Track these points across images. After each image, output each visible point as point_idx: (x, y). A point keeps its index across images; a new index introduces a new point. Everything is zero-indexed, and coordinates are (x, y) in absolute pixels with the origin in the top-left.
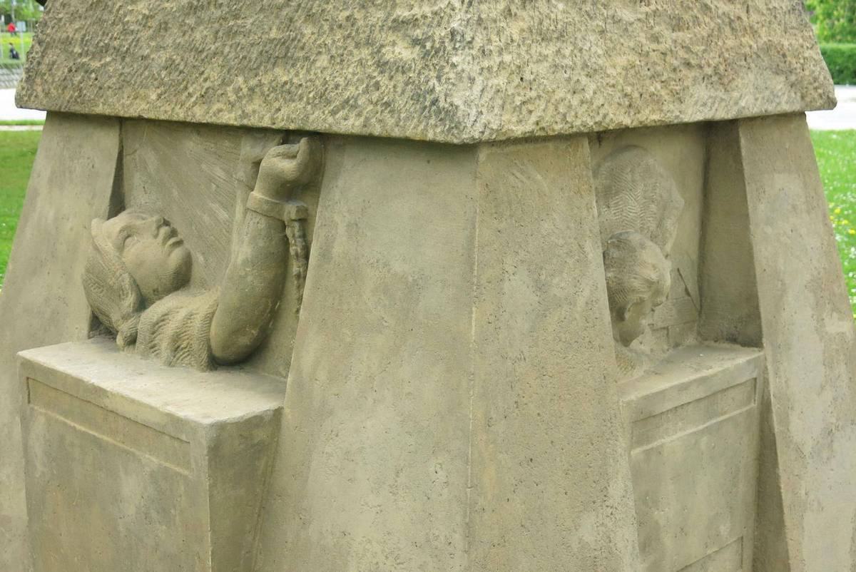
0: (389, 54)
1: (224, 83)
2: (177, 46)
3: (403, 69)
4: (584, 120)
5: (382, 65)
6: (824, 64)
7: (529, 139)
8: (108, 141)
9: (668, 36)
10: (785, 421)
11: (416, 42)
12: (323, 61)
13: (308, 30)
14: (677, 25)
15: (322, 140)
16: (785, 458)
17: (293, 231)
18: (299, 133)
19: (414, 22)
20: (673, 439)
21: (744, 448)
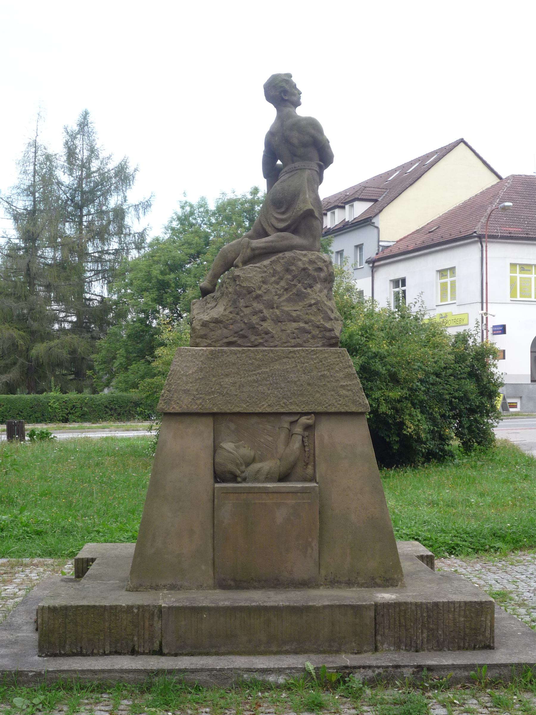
5: (340, 396)
19: (347, 386)
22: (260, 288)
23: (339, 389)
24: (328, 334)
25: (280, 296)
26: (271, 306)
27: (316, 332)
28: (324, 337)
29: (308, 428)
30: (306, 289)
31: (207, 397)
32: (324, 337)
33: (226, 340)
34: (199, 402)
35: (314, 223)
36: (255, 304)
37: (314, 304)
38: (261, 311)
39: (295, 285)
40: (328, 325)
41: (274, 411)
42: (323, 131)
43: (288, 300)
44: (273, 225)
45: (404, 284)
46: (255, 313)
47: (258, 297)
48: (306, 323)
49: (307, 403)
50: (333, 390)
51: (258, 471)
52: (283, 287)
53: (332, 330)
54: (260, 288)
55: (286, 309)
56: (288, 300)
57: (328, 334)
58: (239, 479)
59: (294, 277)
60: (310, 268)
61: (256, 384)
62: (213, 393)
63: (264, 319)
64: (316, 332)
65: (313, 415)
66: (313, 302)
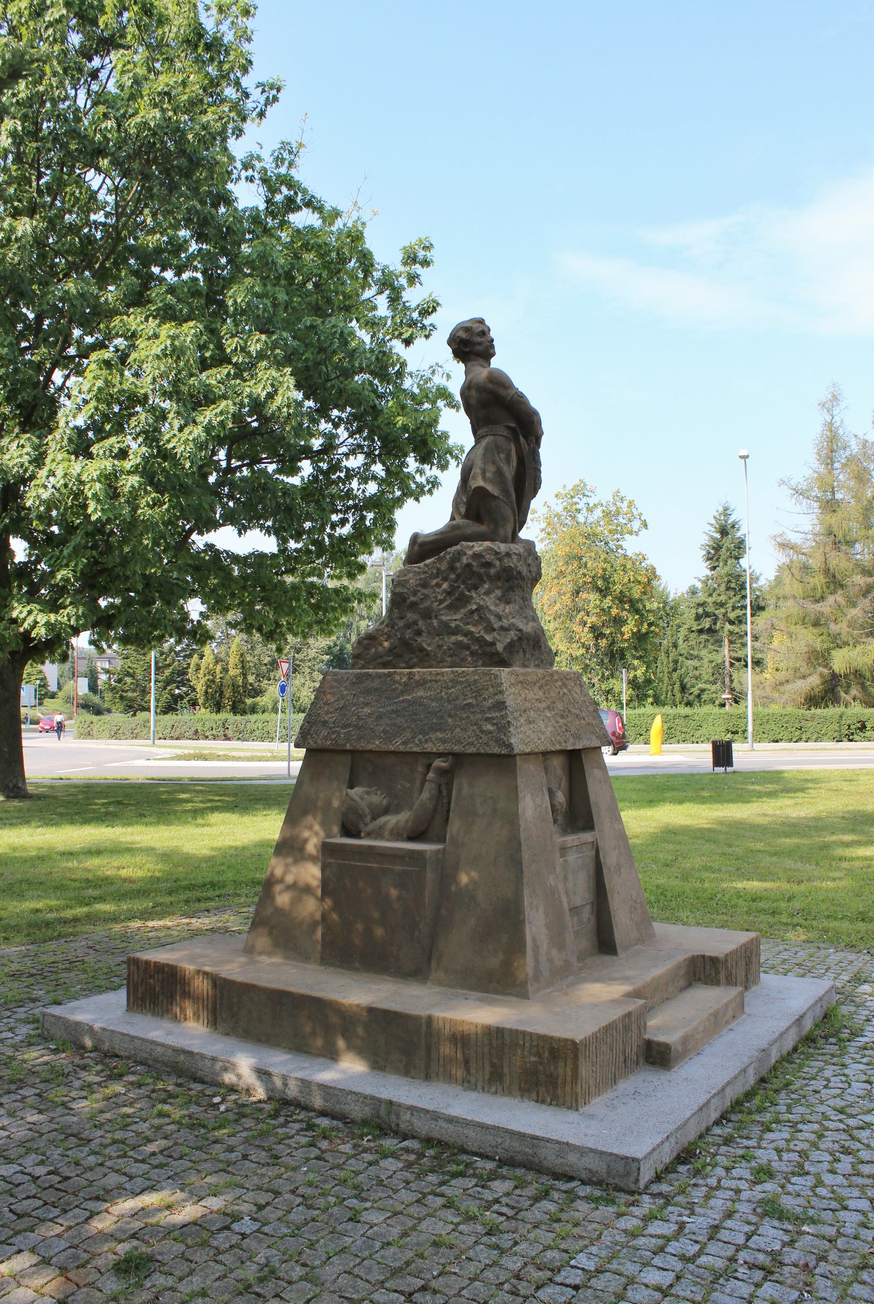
0: (484, 728)
1: (413, 737)
2: (388, 725)
3: (490, 732)
4: (542, 748)
5: (483, 732)
6: (376, 744)
7: (529, 754)
8: (347, 759)
9: (561, 721)
10: (604, 857)
11: (494, 724)
12: (458, 730)
13: (450, 720)
14: (562, 717)
15: (457, 756)
16: (605, 871)
17: (443, 788)
18: (450, 754)
19: (493, 718)
20: (571, 857)
21: (592, 866)
22: (415, 593)
23: (482, 723)
24: (488, 649)
25: (441, 602)
26: (427, 615)
27: (475, 647)
28: (484, 654)
29: (442, 772)
30: (469, 591)
31: (343, 731)
32: (484, 654)
33: (379, 661)
34: (333, 736)
35: (493, 504)
36: (409, 615)
37: (476, 610)
38: (415, 623)
39: (458, 587)
40: (488, 638)
41: (407, 750)
42: (539, 422)
43: (449, 607)
44: (803, 790)
45: (278, 90)
46: (408, 626)
47: (414, 605)
48: (466, 635)
49: (444, 741)
50: (476, 724)
51: (385, 824)
52: (445, 591)
53: (493, 644)
54: (415, 593)
55: (444, 618)
56: (449, 607)
57: (488, 649)
58: (362, 834)
59: (458, 576)
60: (474, 564)
61: (394, 716)
62: (349, 725)
63: (419, 633)
64: (475, 647)
65: (450, 757)
66: (474, 607)
